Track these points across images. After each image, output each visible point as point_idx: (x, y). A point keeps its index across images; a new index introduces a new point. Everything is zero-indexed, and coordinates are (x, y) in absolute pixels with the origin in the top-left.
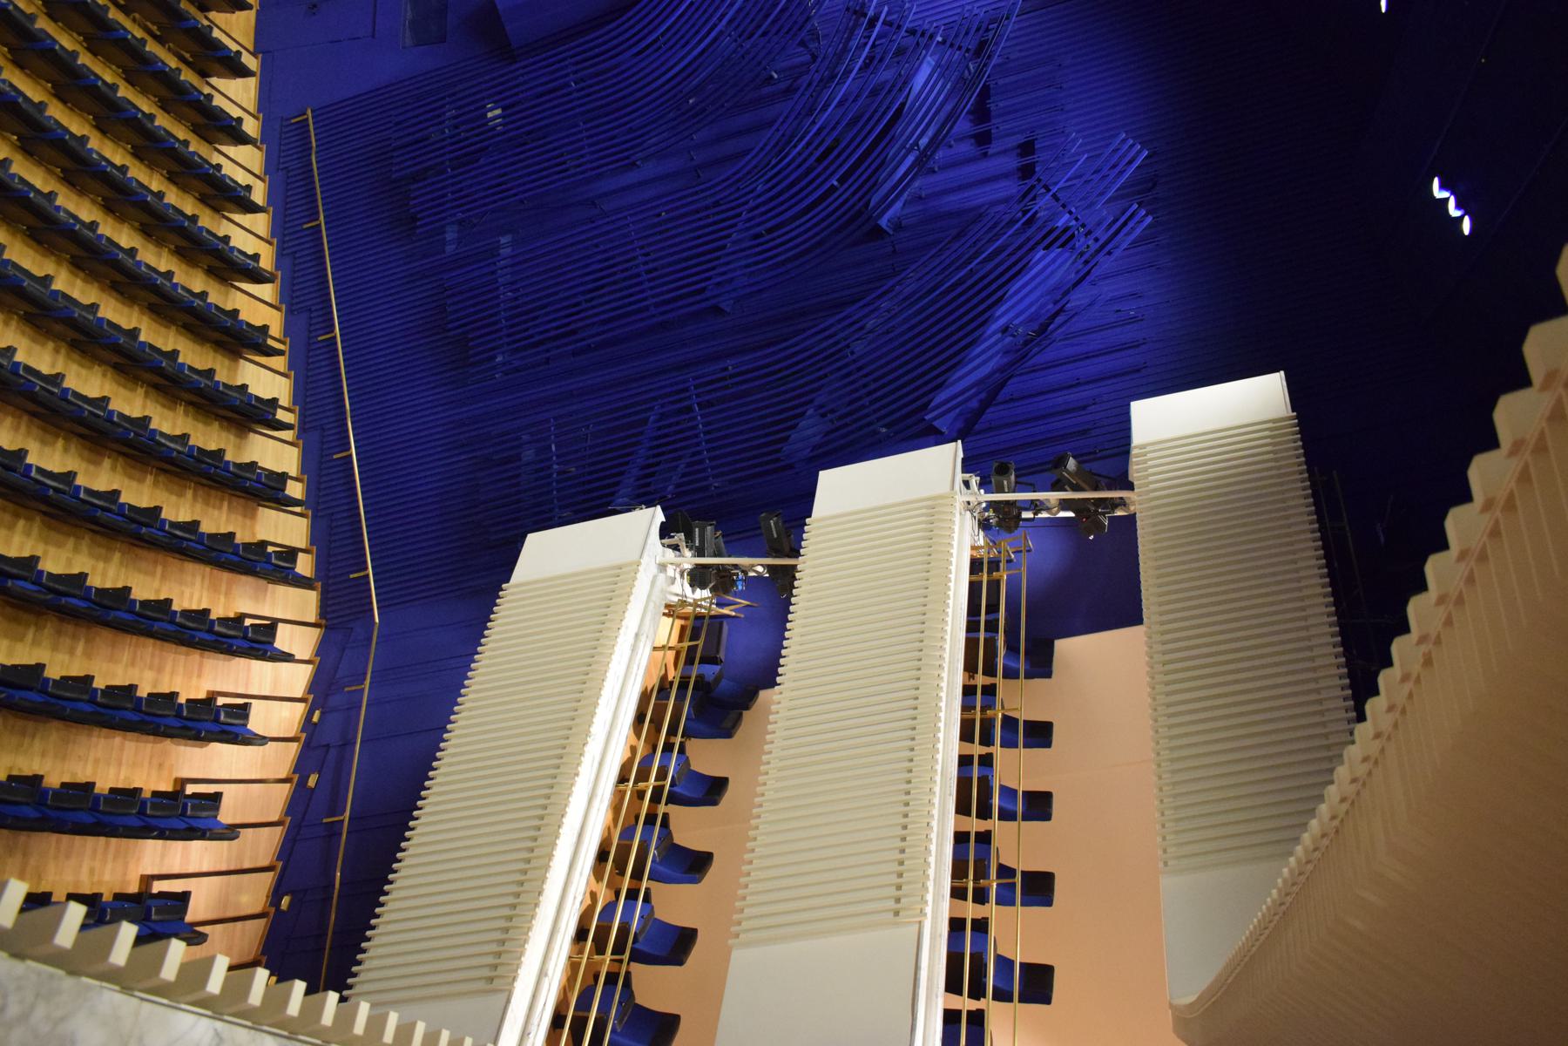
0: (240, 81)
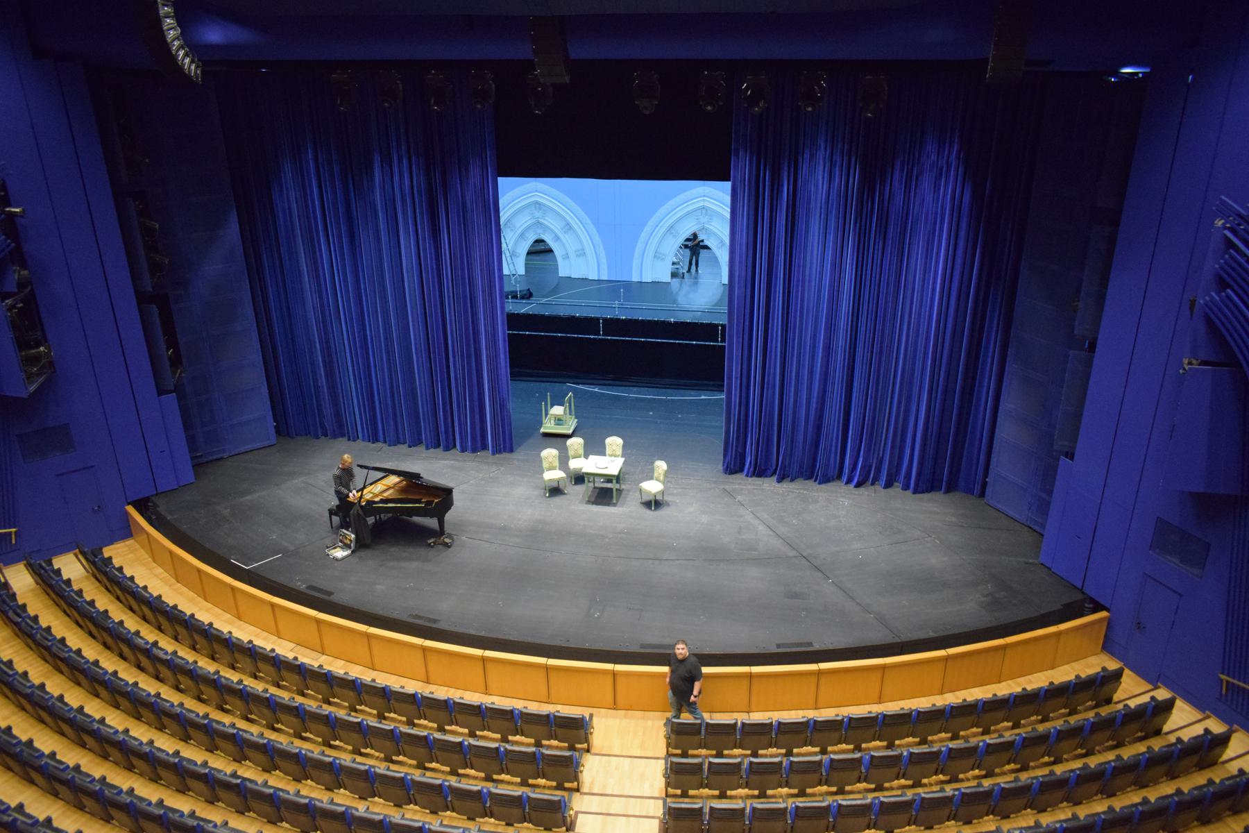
0: (1174, 711)
